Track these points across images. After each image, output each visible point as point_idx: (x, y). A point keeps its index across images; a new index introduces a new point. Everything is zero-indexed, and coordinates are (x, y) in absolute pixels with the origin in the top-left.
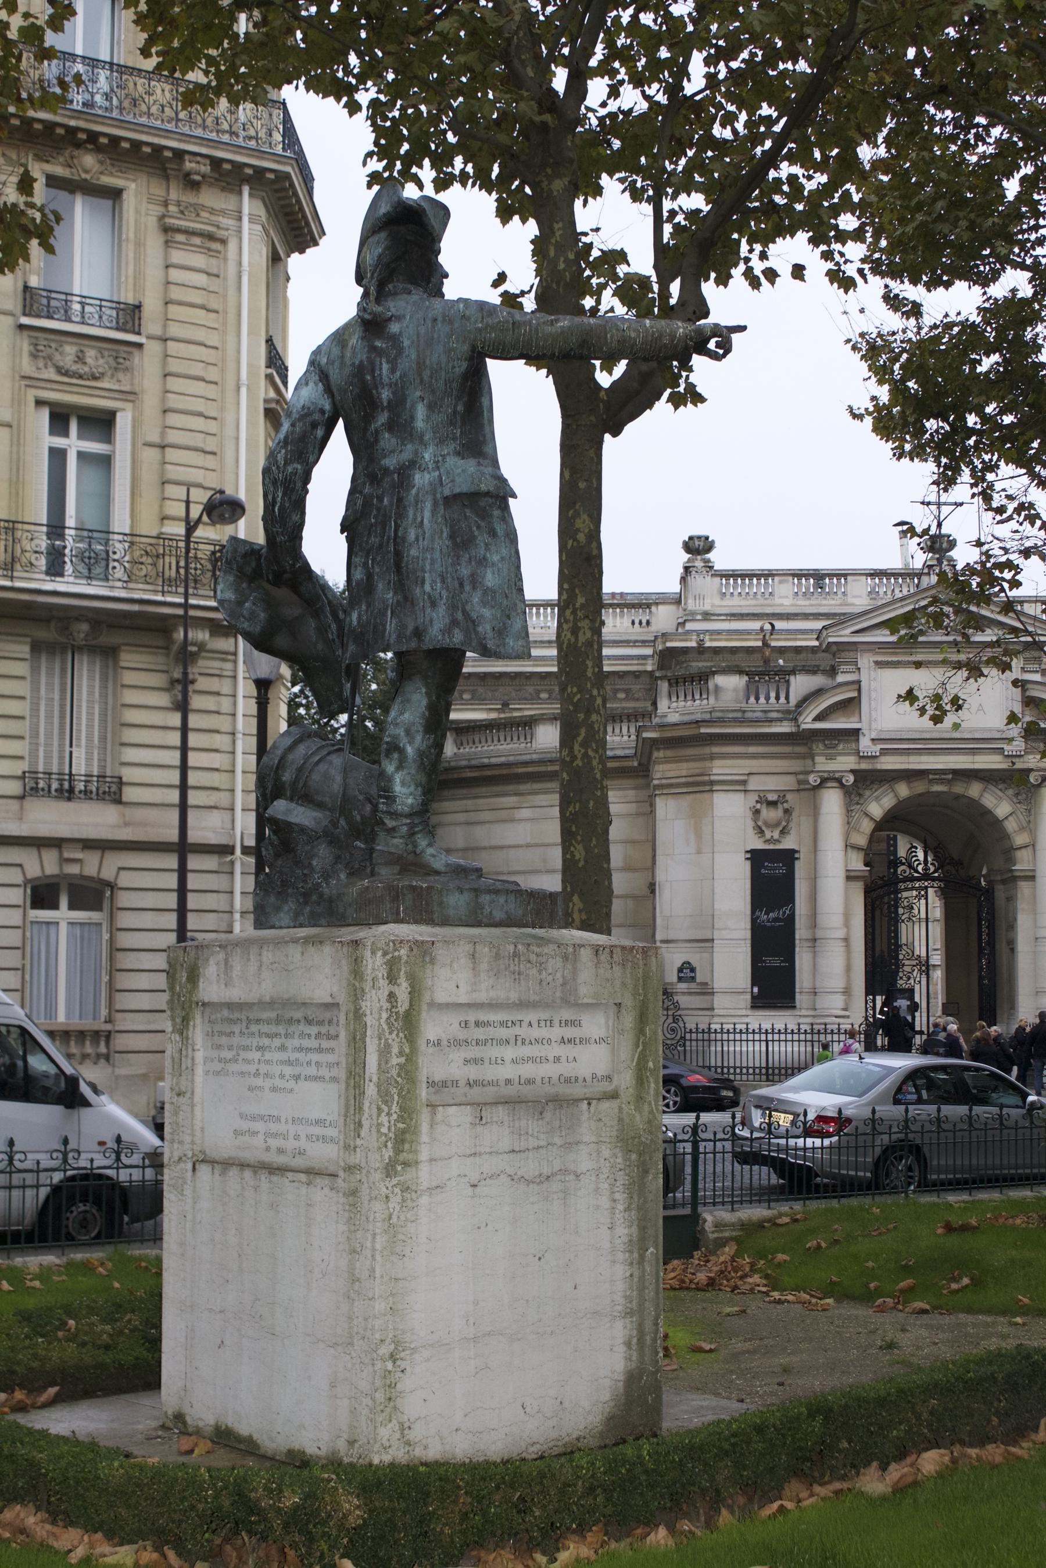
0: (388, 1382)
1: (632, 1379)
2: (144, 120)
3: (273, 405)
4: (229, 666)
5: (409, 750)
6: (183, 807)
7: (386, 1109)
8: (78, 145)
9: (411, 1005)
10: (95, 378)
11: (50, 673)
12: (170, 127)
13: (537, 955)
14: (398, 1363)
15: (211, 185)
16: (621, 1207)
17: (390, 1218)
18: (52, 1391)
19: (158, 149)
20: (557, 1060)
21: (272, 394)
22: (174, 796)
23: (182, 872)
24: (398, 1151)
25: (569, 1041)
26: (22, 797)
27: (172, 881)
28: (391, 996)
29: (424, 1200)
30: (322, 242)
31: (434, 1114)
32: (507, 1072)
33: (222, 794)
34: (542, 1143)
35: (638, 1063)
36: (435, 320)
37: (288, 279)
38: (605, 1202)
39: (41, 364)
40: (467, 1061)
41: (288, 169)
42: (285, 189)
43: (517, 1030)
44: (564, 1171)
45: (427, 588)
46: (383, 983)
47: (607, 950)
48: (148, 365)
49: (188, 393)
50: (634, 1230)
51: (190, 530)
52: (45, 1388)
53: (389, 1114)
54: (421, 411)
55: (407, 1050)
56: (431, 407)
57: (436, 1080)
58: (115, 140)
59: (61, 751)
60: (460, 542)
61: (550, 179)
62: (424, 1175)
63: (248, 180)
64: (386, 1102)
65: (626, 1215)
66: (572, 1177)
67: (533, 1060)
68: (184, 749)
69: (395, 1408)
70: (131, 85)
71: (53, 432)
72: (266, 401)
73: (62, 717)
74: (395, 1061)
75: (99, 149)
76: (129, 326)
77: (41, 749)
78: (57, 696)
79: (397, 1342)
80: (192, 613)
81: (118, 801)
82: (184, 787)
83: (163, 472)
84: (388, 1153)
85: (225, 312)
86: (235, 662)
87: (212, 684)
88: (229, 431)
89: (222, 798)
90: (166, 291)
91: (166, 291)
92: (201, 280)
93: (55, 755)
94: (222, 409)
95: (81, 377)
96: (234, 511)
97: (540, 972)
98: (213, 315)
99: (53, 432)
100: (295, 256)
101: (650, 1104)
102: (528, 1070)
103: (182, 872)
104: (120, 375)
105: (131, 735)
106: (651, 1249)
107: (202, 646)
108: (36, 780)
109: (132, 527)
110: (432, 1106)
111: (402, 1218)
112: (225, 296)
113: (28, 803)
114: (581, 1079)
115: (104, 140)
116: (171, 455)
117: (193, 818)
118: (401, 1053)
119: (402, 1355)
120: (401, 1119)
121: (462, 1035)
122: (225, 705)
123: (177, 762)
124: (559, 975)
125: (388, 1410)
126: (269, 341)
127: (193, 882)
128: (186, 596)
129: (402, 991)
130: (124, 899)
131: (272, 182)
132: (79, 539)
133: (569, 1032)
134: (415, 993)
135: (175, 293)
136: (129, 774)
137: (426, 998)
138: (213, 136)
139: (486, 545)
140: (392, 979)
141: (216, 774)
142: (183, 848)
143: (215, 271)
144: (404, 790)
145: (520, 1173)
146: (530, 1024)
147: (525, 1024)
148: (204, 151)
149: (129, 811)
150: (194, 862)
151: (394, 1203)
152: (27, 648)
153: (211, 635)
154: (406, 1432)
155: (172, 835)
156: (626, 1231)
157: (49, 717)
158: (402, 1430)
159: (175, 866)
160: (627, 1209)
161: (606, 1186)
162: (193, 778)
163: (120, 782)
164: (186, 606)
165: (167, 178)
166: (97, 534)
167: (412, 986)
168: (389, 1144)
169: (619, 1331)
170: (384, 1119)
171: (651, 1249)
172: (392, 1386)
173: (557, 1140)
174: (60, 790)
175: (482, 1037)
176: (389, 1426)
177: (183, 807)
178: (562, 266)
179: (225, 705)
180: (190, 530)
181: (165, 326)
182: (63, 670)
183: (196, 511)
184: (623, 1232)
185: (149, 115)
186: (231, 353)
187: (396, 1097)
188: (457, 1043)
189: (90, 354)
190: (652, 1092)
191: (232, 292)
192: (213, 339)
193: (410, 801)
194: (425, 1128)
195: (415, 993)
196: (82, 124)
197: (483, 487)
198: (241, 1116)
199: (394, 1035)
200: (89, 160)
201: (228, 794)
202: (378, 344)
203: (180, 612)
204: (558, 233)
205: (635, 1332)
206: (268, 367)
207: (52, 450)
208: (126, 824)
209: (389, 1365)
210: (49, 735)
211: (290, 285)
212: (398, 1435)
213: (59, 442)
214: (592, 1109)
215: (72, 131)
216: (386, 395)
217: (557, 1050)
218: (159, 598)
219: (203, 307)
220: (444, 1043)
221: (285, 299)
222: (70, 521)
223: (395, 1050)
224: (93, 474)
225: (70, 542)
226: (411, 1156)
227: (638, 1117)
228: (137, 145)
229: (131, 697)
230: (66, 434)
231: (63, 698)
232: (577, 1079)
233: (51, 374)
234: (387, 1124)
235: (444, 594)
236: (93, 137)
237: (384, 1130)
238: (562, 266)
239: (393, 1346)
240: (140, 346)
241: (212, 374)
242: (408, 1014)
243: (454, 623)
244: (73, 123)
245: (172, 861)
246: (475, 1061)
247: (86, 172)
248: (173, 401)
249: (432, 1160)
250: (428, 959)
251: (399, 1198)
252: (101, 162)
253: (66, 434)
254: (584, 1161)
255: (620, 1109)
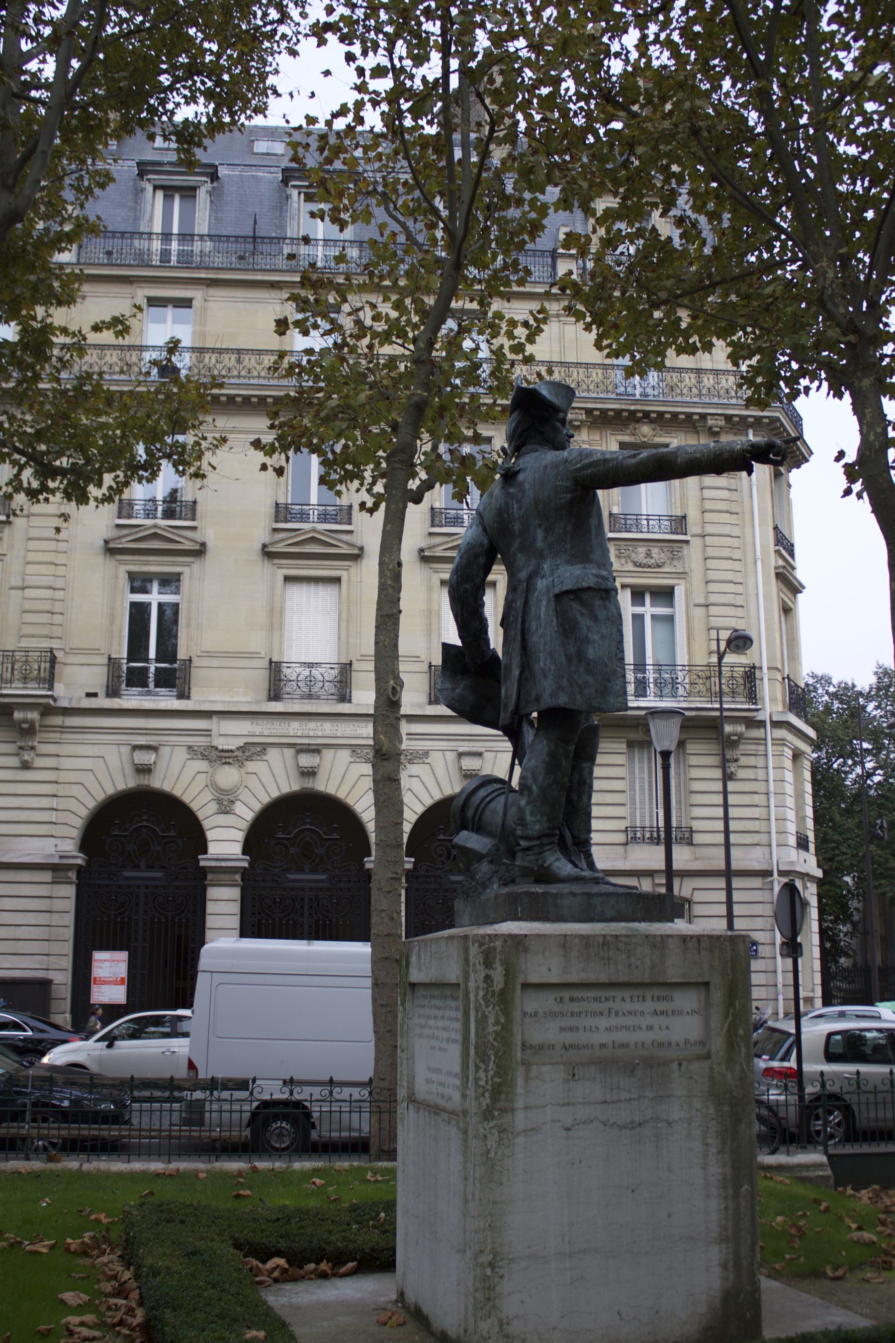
0: (487, 1285)
1: (728, 1296)
2: (679, 399)
3: (781, 570)
4: (762, 748)
5: (534, 788)
6: (727, 845)
7: (483, 1066)
8: (638, 421)
9: (506, 984)
10: (659, 566)
11: (641, 761)
12: (696, 400)
13: (626, 944)
14: (497, 1270)
15: (727, 433)
16: (713, 1150)
17: (488, 1152)
18: (351, 1265)
19: (689, 415)
20: (650, 1028)
21: (781, 563)
22: (720, 839)
23: (729, 890)
24: (495, 1098)
25: (662, 1013)
26: (627, 844)
27: (722, 896)
28: (488, 978)
29: (520, 1140)
30: (812, 459)
31: (528, 1070)
32: (598, 1038)
33: (762, 835)
34: (633, 1096)
35: (728, 1031)
36: (546, 467)
37: (790, 486)
38: (697, 1145)
39: (623, 561)
40: (562, 1029)
41: (777, 414)
42: (777, 428)
43: (611, 1004)
44: (657, 1119)
45: (541, 664)
46: (480, 968)
47: (694, 939)
48: (693, 554)
49: (721, 569)
50: (728, 1170)
51: (720, 658)
52: (346, 1263)
53: (486, 1071)
54: (540, 534)
55: (503, 1020)
56: (547, 530)
57: (534, 1043)
58: (661, 414)
59: (651, 812)
60: (568, 628)
61: (860, 379)
62: (520, 1120)
63: (751, 426)
64: (483, 1062)
65: (720, 1157)
66: (664, 1124)
67: (627, 1028)
68: (726, 806)
69: (494, 1306)
70: (669, 378)
71: (634, 604)
72: (776, 568)
73: (650, 790)
74: (491, 1029)
75: (652, 421)
76: (679, 530)
77: (638, 812)
78: (646, 776)
79: (496, 1254)
80: (725, 714)
81: (691, 844)
82: (727, 832)
83: (708, 622)
84: (486, 1101)
85: (743, 513)
86: (766, 745)
87: (751, 761)
88: (751, 591)
89: (763, 838)
90: (702, 504)
91: (702, 504)
92: (725, 494)
93: (647, 815)
94: (746, 577)
95: (649, 567)
96: (745, 643)
97: (629, 957)
98: (735, 516)
99: (634, 604)
100: (794, 470)
101: (741, 1064)
102: (621, 1037)
103: (729, 890)
104: (676, 563)
105: (697, 799)
106: (746, 1187)
107: (741, 736)
108: (635, 833)
109: (689, 660)
110: (527, 1065)
111: (500, 1153)
112: (742, 503)
113: (630, 848)
114: (674, 1044)
115: (654, 415)
116: (713, 610)
117: (735, 852)
118: (497, 1023)
119: (500, 1263)
120: (497, 1074)
121: (557, 1008)
122: (761, 774)
123: (722, 815)
124: (647, 960)
125: (488, 1308)
126: (776, 528)
127: (736, 896)
128: (721, 703)
129: (498, 974)
130: (697, 910)
131: (768, 424)
132: (655, 671)
133: (661, 1006)
134: (510, 974)
135: (708, 505)
136: (696, 825)
137: (521, 979)
138: (725, 401)
139: (588, 627)
140: (488, 963)
141: (757, 822)
142: (728, 873)
143: (734, 487)
144: (533, 819)
145: (612, 1120)
146: (623, 999)
147: (618, 1000)
148: (719, 411)
149: (698, 850)
150: (736, 883)
151: (492, 1142)
152: (624, 746)
153: (747, 728)
154: (505, 1327)
155: (722, 865)
156: (720, 1171)
157: (642, 790)
158: (501, 1325)
159: (724, 886)
160: (721, 1152)
161: (698, 1132)
162: (733, 826)
163: (691, 831)
164: (721, 709)
165: (698, 433)
166: (668, 666)
167: (507, 970)
168: (487, 1095)
169: (716, 1254)
170: (482, 1074)
171: (746, 1187)
172: (491, 1288)
173: (648, 1094)
174: (651, 838)
175: (576, 1010)
176: (489, 1321)
177: (727, 845)
178: (872, 438)
179: (761, 774)
180: (720, 658)
181: (703, 527)
182: (649, 758)
183: (723, 645)
184: (715, 1171)
185: (682, 394)
186: (749, 539)
187: (493, 1058)
188: (553, 1015)
189: (655, 551)
190: (743, 1054)
191: (746, 499)
192: (736, 532)
193: (538, 827)
194: (520, 1082)
195: (510, 974)
196: (638, 407)
197: (585, 584)
198: (429, 1069)
199: (490, 1008)
200: (646, 429)
201: (766, 835)
202: (511, 491)
203: (717, 714)
204: (868, 416)
205: (731, 1257)
206: (776, 545)
207: (634, 616)
208: (697, 859)
209: (488, 1271)
210: (642, 802)
211: (792, 490)
212: (497, 1329)
213: (639, 610)
214: (683, 1068)
215: (632, 413)
216: (517, 526)
217: (650, 1020)
218: (709, 706)
219: (728, 512)
220: (541, 1014)
221: (789, 499)
222: (649, 661)
223: (492, 1020)
224: (662, 628)
225: (651, 676)
226: (507, 1105)
227: (729, 1075)
228: (675, 415)
229: (695, 773)
230: (643, 605)
231: (650, 777)
232: (670, 1044)
233: (630, 567)
234: (484, 1079)
235: (552, 667)
236: (646, 414)
237: (482, 1083)
238: (872, 438)
239: (491, 1256)
240: (687, 542)
241: (737, 554)
242: (503, 992)
243: (560, 688)
244: (633, 408)
245: (721, 883)
246: (571, 1029)
247: (644, 437)
248: (712, 575)
249: (526, 1108)
250: (521, 949)
251: (496, 1138)
252: (654, 430)
253: (643, 605)
254: (676, 1111)
255: (711, 1069)
